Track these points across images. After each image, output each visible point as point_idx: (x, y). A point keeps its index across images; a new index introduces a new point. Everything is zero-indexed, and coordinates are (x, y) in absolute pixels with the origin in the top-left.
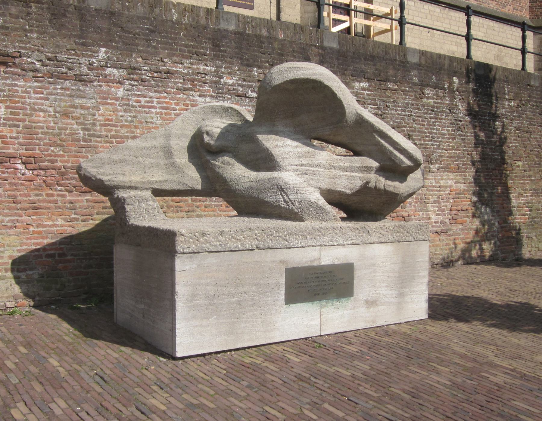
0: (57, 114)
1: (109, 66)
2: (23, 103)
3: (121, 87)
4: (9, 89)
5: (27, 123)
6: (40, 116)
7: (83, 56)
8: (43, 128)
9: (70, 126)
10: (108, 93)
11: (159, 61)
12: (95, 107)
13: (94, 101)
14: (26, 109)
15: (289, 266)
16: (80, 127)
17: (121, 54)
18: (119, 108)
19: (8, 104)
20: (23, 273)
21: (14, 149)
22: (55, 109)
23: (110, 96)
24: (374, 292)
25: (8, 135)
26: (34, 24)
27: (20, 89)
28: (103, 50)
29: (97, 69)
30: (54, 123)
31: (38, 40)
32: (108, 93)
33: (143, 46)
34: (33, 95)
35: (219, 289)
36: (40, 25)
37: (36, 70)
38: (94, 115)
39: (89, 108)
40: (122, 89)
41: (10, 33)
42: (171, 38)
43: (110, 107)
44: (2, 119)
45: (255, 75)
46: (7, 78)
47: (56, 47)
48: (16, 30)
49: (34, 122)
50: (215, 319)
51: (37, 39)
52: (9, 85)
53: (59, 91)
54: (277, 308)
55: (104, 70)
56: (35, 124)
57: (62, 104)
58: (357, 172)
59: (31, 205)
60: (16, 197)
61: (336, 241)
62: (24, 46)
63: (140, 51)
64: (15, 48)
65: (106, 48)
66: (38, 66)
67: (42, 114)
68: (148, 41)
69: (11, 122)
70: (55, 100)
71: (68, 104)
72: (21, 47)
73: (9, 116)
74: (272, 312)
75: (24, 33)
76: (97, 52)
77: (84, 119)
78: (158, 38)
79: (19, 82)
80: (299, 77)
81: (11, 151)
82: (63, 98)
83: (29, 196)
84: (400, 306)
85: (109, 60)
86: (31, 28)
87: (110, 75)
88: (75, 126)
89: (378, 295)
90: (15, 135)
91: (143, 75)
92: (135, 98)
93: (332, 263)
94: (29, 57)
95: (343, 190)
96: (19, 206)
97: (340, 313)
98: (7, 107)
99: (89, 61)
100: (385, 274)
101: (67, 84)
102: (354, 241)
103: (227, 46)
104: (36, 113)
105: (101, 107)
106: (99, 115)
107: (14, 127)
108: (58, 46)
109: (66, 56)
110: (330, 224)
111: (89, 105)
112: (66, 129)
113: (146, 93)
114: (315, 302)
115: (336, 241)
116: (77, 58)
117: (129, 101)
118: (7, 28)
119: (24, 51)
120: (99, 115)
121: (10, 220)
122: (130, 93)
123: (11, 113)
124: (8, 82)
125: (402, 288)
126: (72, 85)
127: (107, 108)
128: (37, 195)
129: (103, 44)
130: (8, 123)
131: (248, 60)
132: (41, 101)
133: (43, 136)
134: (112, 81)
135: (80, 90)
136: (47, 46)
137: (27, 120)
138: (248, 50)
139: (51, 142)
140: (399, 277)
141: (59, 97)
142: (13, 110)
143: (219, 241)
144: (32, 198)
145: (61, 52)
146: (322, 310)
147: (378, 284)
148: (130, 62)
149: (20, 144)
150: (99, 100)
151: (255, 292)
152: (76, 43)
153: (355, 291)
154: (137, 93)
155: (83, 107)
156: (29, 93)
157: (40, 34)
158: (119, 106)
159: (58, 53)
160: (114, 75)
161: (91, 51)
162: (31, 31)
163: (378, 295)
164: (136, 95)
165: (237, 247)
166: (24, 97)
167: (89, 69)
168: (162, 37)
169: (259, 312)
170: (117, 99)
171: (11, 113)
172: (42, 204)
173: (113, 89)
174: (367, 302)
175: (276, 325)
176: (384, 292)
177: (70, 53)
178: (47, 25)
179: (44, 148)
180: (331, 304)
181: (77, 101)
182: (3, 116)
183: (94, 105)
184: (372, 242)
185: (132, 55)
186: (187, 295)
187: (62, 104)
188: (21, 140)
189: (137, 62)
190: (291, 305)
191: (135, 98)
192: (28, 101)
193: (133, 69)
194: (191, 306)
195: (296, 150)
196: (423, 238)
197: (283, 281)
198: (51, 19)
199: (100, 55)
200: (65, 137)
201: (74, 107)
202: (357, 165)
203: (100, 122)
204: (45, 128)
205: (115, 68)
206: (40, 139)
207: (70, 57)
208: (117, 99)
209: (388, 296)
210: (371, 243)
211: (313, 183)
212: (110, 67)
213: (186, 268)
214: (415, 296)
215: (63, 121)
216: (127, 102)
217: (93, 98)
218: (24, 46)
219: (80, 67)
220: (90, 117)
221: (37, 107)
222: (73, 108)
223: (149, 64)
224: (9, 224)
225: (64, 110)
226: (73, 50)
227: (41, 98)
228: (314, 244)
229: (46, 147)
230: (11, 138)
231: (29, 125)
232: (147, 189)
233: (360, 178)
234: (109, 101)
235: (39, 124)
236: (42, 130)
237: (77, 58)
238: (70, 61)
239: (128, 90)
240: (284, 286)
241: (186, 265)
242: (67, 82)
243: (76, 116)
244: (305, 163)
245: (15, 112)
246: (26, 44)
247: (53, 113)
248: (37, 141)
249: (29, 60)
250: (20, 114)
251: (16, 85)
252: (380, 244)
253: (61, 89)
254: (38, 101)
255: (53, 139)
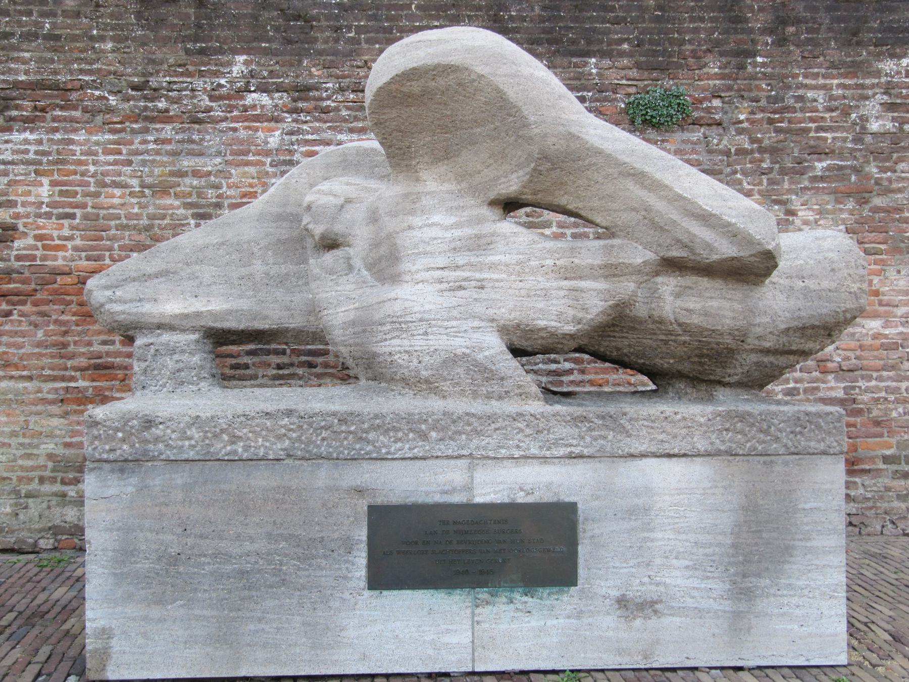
0: (146, 191)
1: (252, 89)
2: (83, 174)
3: (278, 129)
4: (57, 149)
5: (89, 209)
6: (113, 196)
7: (201, 74)
8: (120, 218)
9: (170, 212)
10: (250, 141)
11: (358, 67)
12: (221, 172)
13: (218, 160)
14: (88, 184)
15: (379, 501)
16: (190, 212)
17: (277, 63)
18: (270, 170)
19: (56, 177)
20: (72, 487)
21: (65, 258)
22: (142, 181)
23: (253, 148)
24: (646, 580)
25: (55, 234)
26: (106, 25)
27: (78, 148)
28: (242, 58)
29: (228, 97)
30: (140, 208)
31: (115, 55)
32: (250, 141)
33: (326, 42)
34: (102, 158)
35: (190, 541)
36: (118, 25)
37: (110, 110)
38: (218, 187)
39: (209, 173)
40: (277, 133)
41: (63, 47)
42: (388, 19)
43: (252, 170)
44: (44, 206)
45: (591, 74)
46: (56, 130)
47: (148, 64)
48: (74, 38)
49: (103, 208)
50: (181, 606)
51: (113, 51)
52: (60, 142)
53: (152, 146)
54: (347, 595)
55: (242, 98)
56: (105, 212)
57: (156, 171)
58: (595, 278)
59: (92, 361)
60: (65, 345)
61: (518, 447)
62: (88, 67)
63: (320, 53)
64: (71, 73)
65: (248, 54)
66: (114, 103)
67: (117, 192)
68: (337, 29)
69: (61, 210)
70: (144, 163)
71: (168, 169)
72: (81, 71)
73: (58, 199)
74: (331, 604)
75: (90, 43)
76: (230, 64)
77: (199, 195)
78: (359, 21)
79: (77, 135)
80: (420, 63)
81: (60, 262)
82: (158, 158)
83: (90, 344)
84: (738, 623)
85: (252, 77)
86: (101, 33)
87: (254, 107)
88: (182, 211)
89: (662, 589)
90: (66, 232)
91: (323, 99)
92: (303, 149)
93: (507, 500)
94: (97, 88)
95: (553, 324)
96: (69, 363)
97: (534, 623)
98: (53, 184)
99: (212, 83)
100: (684, 537)
101: (168, 131)
102: (577, 450)
103: (523, 19)
104: (106, 189)
105: (233, 171)
106: (229, 187)
107: (67, 218)
108: (153, 62)
109: (168, 79)
110: (510, 407)
111: (210, 169)
112: (163, 217)
113: (328, 135)
114: (458, 591)
115: (518, 447)
116: (189, 80)
117: (293, 155)
118: (57, 38)
119: (87, 78)
120: (229, 187)
121: (53, 389)
122: (294, 138)
123: (61, 193)
124: (58, 136)
125: (744, 576)
126: (177, 133)
127: (245, 173)
128: (104, 343)
129: (242, 47)
130: (55, 211)
131: (573, 42)
132: (116, 167)
133: (119, 232)
134: (257, 118)
135: (192, 142)
136: (130, 63)
137: (90, 204)
138: (576, 19)
139: (133, 243)
140: (734, 546)
141: (151, 158)
142: (64, 188)
143: (190, 439)
144: (96, 348)
145: (158, 72)
146: (477, 611)
147: (658, 561)
148: (297, 77)
149: (76, 249)
150: (231, 158)
151: (286, 555)
152: (187, 52)
153: (582, 572)
154: (310, 137)
155: (196, 174)
156: (95, 154)
157: (119, 42)
158: (271, 165)
159: (151, 74)
160: (263, 107)
161: (216, 65)
162: (102, 39)
163: (662, 589)
164: (307, 142)
165: (235, 452)
166: (84, 163)
167: (212, 98)
168: (370, 18)
169: (295, 601)
170: (267, 153)
171: (61, 193)
172: (113, 360)
173: (260, 134)
174: (622, 602)
175: (343, 634)
176: (679, 581)
177: (175, 71)
178: (132, 25)
179: (119, 255)
180: (504, 600)
181: (187, 163)
182: (46, 200)
183: (220, 168)
184: (636, 452)
185: (300, 62)
186: (114, 551)
187: (156, 171)
188: (78, 242)
189: (311, 75)
190: (385, 593)
191: (303, 149)
192: (92, 168)
193: (302, 91)
194: (122, 574)
195: (448, 235)
196: (822, 446)
197: (362, 534)
198: (139, 12)
199: (235, 69)
200: (159, 232)
201: (182, 174)
202: (590, 261)
203: (230, 201)
204: (123, 219)
205: (265, 92)
206: (113, 239)
207: (176, 79)
208: (267, 153)
209: (695, 593)
210: (632, 456)
211: (479, 309)
212: (254, 91)
213: (111, 492)
214: (795, 600)
215: (157, 202)
216: (288, 158)
217: (219, 153)
218: (88, 67)
219: (194, 97)
220: (211, 192)
221: (108, 180)
222: (177, 176)
223: (338, 77)
224: (50, 396)
225: (160, 182)
226: (180, 66)
227: (116, 163)
228: (450, 452)
229: (123, 253)
230: (60, 238)
231: (93, 214)
232: (194, 330)
233: (600, 292)
234: (251, 158)
235: (111, 211)
236: (118, 222)
237: (189, 80)
238: (175, 87)
239: (291, 133)
240: (364, 547)
241: (109, 486)
242: (168, 127)
243: (183, 192)
244: (461, 263)
245: (67, 190)
246: (91, 64)
247: (137, 189)
248: (108, 243)
249: (97, 93)
250: (77, 193)
251: (71, 142)
252: (665, 460)
253: (155, 141)
254: (111, 167)
255: (137, 238)
